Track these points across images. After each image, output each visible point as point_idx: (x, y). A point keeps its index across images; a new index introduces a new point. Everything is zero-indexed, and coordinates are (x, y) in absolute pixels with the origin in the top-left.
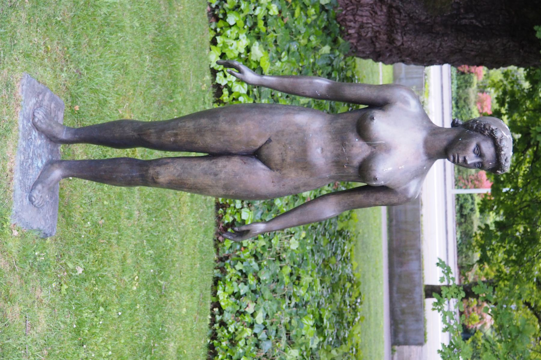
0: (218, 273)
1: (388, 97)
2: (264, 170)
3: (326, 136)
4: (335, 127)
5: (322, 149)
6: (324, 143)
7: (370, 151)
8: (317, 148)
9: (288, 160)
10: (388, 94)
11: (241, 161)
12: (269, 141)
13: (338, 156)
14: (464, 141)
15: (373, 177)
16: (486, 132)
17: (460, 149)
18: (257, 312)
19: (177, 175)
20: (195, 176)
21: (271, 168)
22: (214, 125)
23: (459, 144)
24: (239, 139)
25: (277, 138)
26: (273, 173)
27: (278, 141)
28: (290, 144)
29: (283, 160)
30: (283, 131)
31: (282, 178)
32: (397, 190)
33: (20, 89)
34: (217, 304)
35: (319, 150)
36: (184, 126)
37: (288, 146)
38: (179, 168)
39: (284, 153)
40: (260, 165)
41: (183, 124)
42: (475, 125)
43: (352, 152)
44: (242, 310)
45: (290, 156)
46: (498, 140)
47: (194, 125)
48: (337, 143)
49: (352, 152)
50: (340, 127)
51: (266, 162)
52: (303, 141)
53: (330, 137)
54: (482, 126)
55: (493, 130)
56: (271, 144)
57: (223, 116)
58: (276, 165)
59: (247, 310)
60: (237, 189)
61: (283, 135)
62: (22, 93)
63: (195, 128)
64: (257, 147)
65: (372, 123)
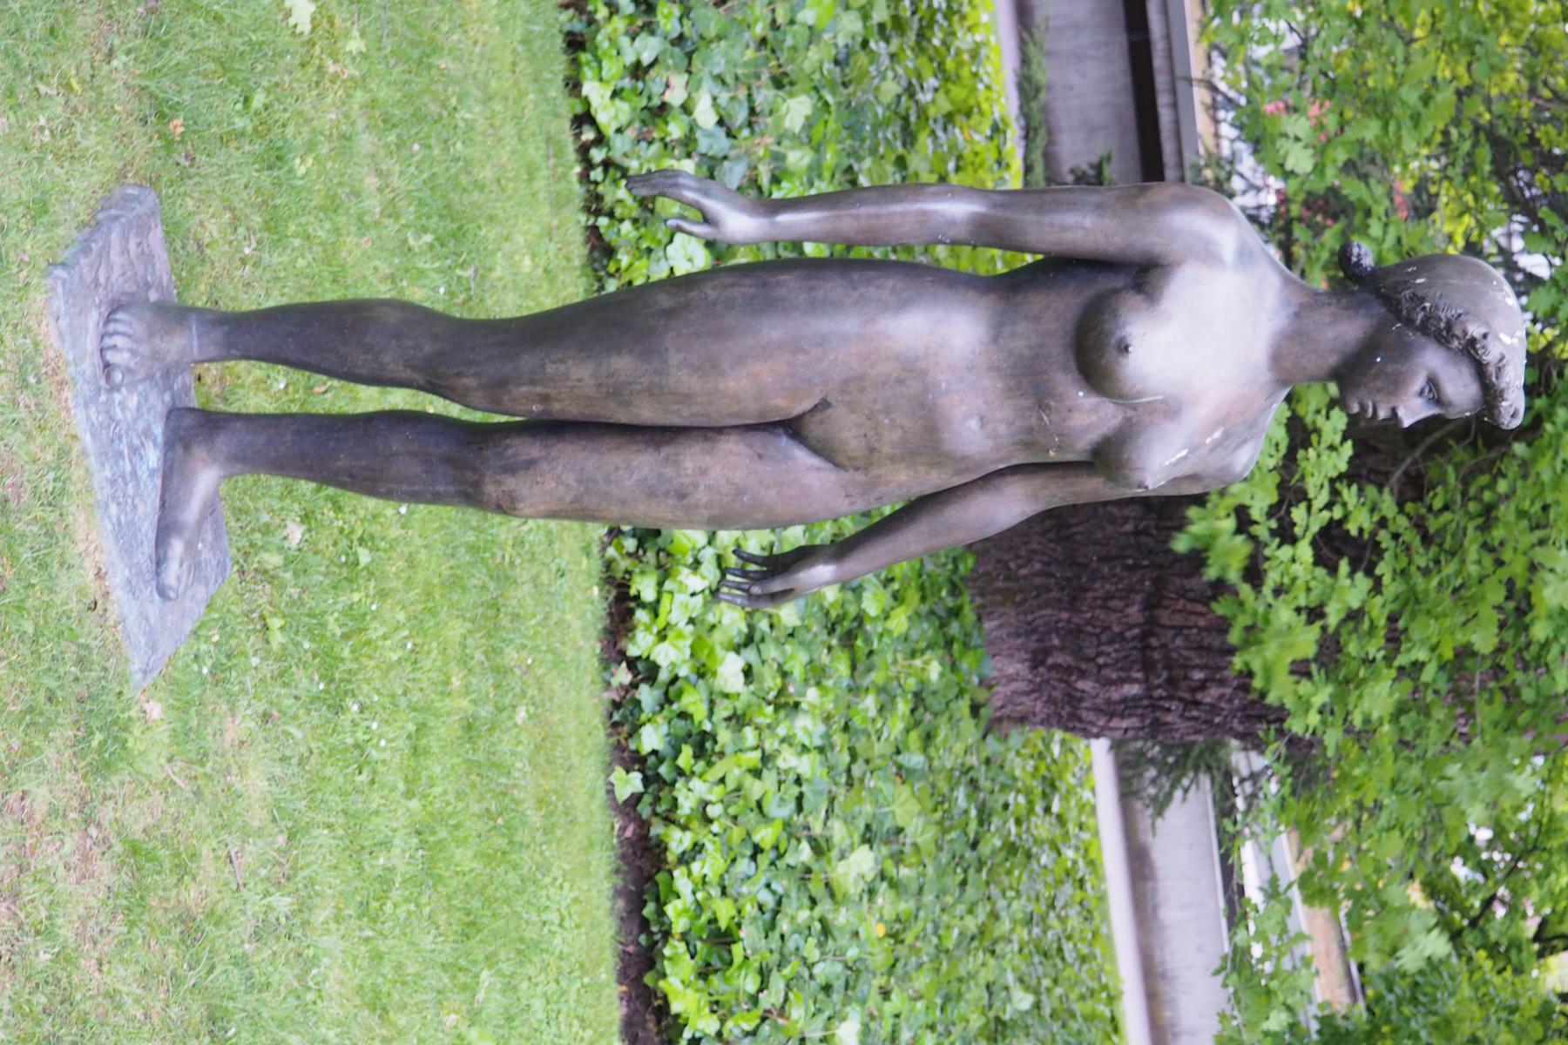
0: (571, 20)
1: (1158, 249)
2: (818, 469)
3: (992, 385)
4: (1010, 352)
5: (982, 418)
6: (986, 403)
7: (1120, 418)
8: (966, 418)
9: (886, 449)
10: (1157, 240)
11: (748, 451)
12: (824, 405)
14: (1390, 369)
16: (1456, 343)
17: (1379, 391)
18: (694, 95)
19: (568, 499)
20: (623, 503)
21: (837, 465)
22: (657, 379)
23: (1377, 376)
25: (847, 398)
26: (846, 476)
27: (852, 407)
28: (888, 411)
29: (872, 450)
30: (861, 378)
31: (873, 484)
33: (52, 330)
34: (584, 118)
35: (974, 424)
36: (566, 376)
37: (881, 417)
38: (570, 479)
39: (871, 433)
40: (802, 457)
41: (562, 368)
42: (1420, 316)
43: (1071, 423)
44: (656, 102)
45: (890, 440)
46: (1492, 369)
47: (593, 376)
48: (1025, 402)
49: (1071, 423)
50: (1026, 352)
51: (824, 451)
52: (923, 406)
53: (1000, 385)
54: (1442, 325)
55: (1473, 341)
56: (830, 411)
57: (678, 350)
58: (851, 459)
59: (668, 97)
61: (862, 390)
62: (63, 341)
63: (599, 386)
65: (1123, 361)
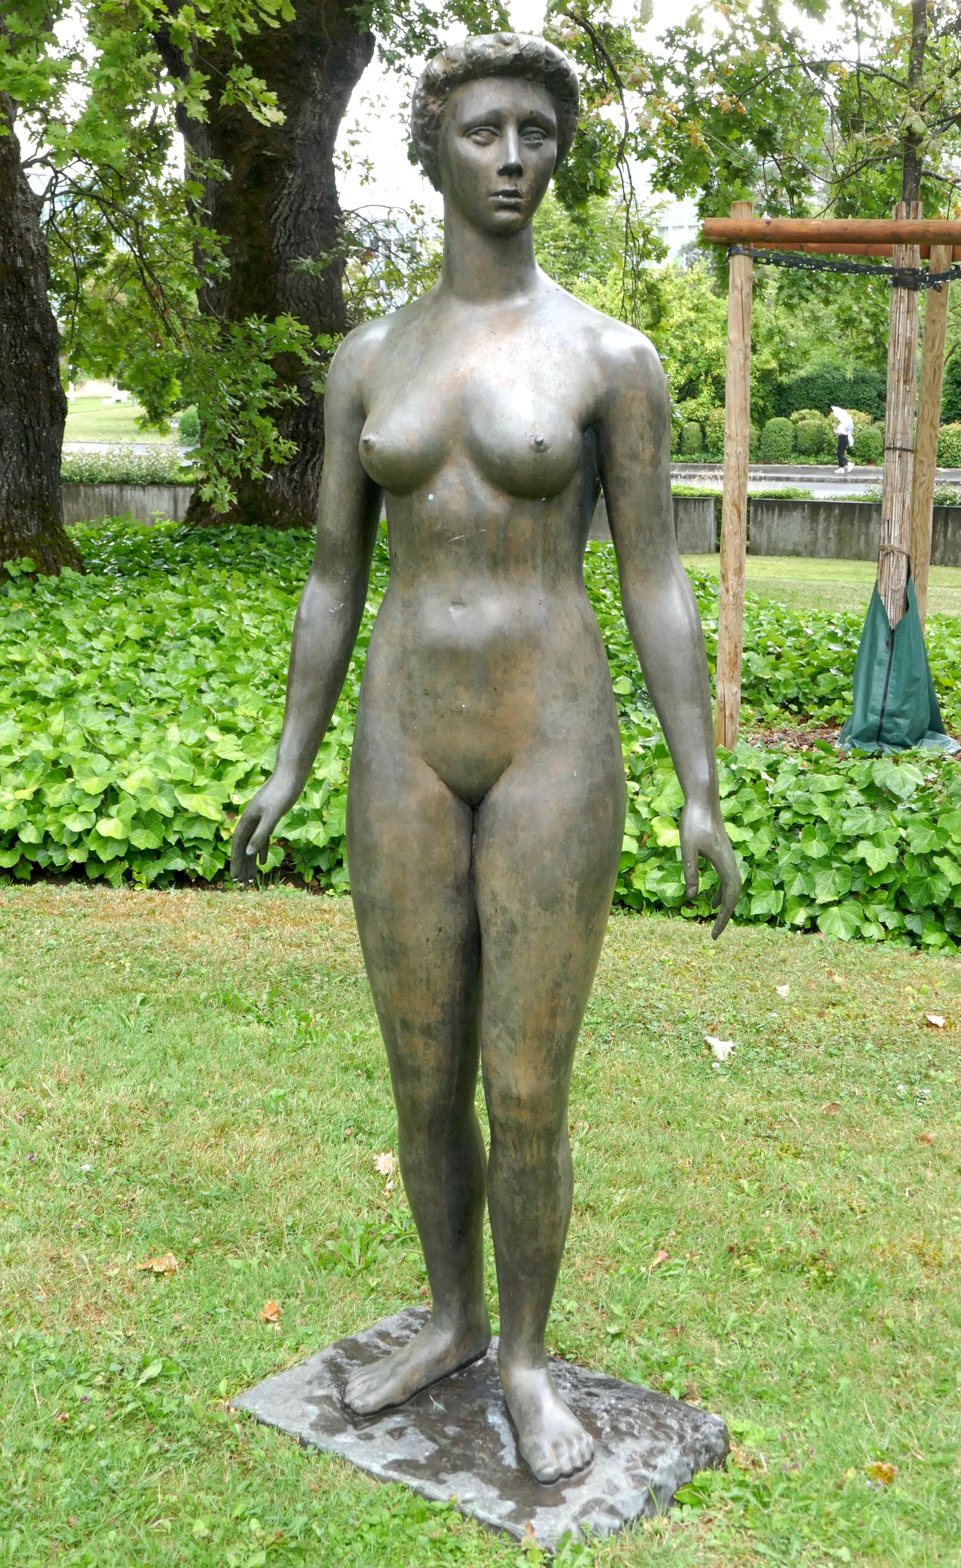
5: (454, 603)
13: (474, 556)
15: (533, 455)
16: (433, 108)
17: (475, 189)
24: (415, 846)
30: (402, 714)
32: (601, 389)
60: (558, 873)
63: (387, 967)
64: (448, 793)
65: (378, 446)
